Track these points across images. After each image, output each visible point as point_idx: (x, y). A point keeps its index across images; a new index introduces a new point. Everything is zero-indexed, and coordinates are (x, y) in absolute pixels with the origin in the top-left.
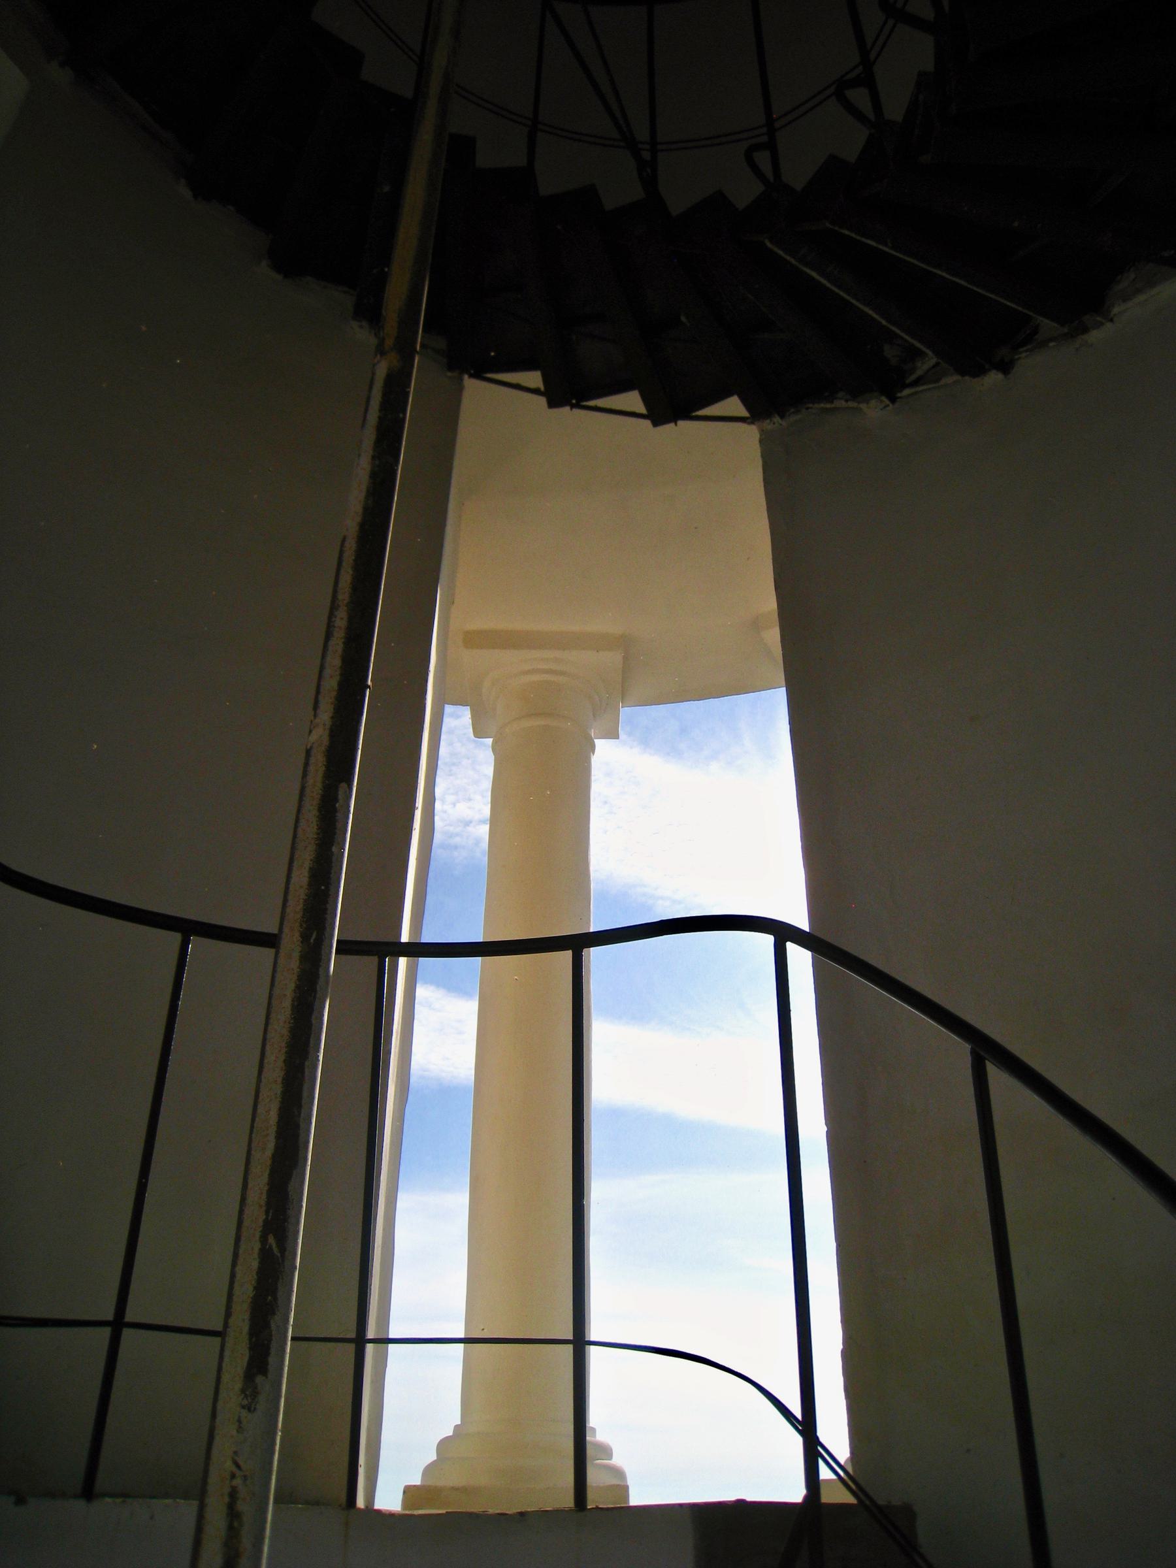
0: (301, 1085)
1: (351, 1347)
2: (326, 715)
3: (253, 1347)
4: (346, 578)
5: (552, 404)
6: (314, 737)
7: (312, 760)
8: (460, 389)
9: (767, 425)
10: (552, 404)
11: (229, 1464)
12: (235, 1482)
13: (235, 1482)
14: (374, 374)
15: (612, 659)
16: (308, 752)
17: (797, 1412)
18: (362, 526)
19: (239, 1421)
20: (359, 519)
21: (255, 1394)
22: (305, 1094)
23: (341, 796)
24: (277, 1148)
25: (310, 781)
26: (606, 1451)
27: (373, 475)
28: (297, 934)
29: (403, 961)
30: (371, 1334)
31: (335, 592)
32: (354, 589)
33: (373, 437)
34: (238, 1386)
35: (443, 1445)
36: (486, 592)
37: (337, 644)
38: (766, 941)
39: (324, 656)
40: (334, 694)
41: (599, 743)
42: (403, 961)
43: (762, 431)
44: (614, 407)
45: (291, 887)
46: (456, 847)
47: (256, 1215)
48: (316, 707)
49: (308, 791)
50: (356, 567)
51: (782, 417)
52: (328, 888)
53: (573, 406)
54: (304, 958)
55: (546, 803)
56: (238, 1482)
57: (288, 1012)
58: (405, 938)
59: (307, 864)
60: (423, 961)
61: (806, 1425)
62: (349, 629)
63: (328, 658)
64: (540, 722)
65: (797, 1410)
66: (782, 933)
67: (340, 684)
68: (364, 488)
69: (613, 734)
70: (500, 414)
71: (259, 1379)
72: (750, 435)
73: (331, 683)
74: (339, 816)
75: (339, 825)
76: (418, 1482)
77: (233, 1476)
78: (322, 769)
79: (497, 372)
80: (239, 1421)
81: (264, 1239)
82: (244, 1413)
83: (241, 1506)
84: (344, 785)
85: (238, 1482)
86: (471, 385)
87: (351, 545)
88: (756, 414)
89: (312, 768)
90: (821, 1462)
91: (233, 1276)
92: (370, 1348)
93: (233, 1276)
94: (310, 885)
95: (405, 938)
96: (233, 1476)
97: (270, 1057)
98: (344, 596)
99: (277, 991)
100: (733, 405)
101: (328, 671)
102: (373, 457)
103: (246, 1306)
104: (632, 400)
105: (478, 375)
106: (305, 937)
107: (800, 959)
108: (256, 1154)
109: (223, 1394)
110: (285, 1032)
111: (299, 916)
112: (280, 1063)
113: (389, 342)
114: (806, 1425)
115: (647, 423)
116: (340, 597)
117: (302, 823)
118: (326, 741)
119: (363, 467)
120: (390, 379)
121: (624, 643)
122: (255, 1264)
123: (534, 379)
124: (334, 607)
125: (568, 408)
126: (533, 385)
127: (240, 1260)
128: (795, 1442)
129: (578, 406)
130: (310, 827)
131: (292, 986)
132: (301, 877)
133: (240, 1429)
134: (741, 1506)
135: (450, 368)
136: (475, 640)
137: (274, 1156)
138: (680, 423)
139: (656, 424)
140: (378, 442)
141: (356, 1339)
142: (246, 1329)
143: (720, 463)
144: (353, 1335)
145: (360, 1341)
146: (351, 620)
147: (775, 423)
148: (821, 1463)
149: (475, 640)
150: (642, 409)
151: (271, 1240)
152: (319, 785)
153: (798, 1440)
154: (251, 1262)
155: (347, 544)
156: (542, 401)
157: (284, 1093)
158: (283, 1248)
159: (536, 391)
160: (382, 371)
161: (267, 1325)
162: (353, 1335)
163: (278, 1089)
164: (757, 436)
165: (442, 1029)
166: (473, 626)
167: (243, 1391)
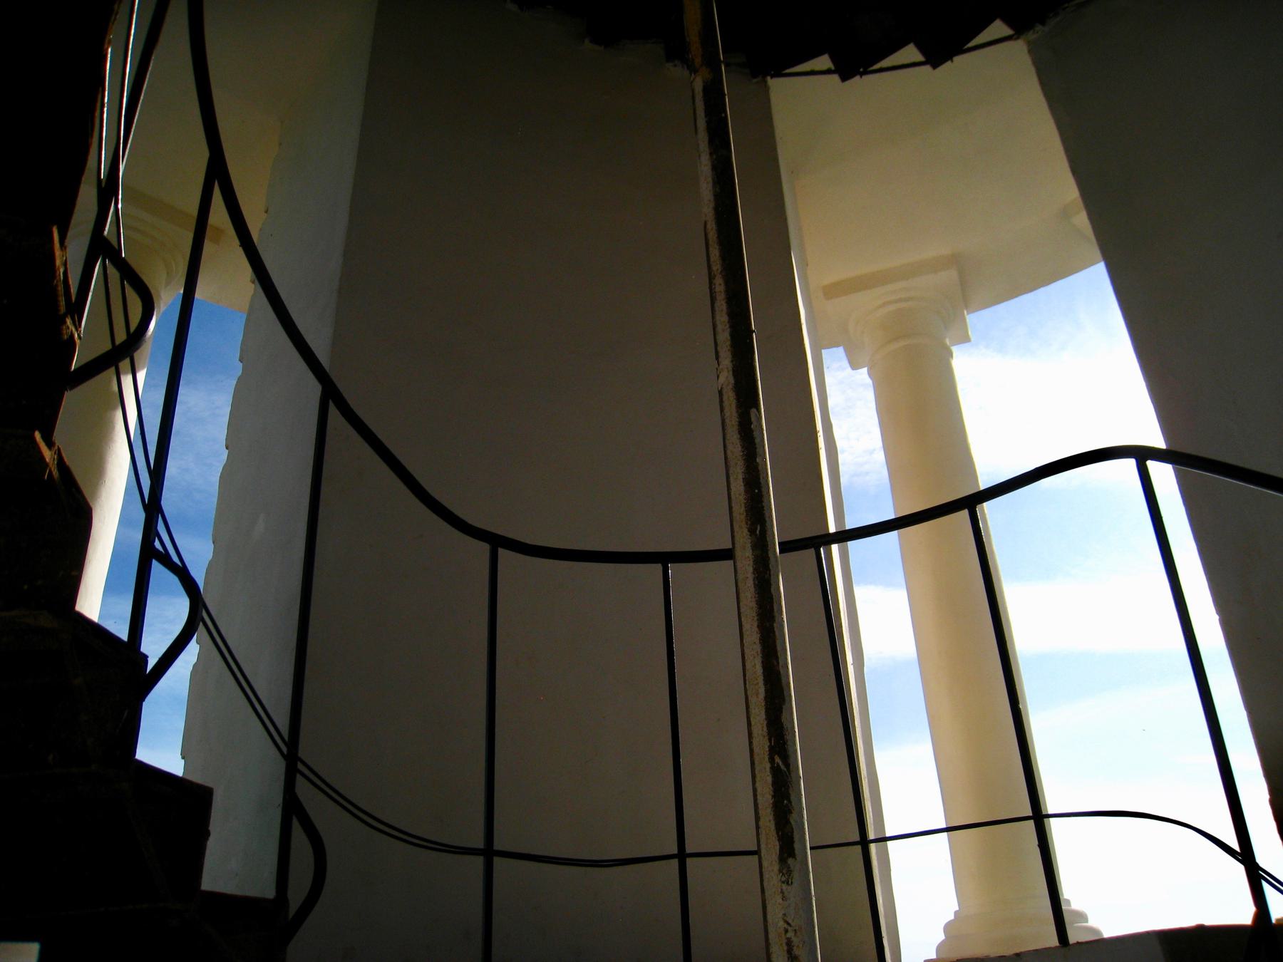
0: (774, 642)
1: (858, 848)
2: (726, 361)
3: (780, 839)
4: (715, 252)
5: (844, 78)
6: (722, 379)
7: (725, 398)
8: (766, 90)
9: (1031, 36)
10: (844, 78)
11: (781, 924)
12: (789, 935)
13: (789, 935)
14: (693, 91)
15: (949, 276)
16: (720, 393)
17: (1235, 845)
18: (716, 209)
19: (782, 892)
20: (712, 205)
21: (790, 872)
22: (779, 648)
23: (753, 419)
24: (766, 691)
25: (727, 414)
26: (1082, 916)
27: (714, 168)
28: (746, 531)
29: (835, 547)
30: (871, 836)
31: (709, 267)
32: (723, 258)
33: (706, 139)
34: (776, 867)
35: (948, 927)
36: (834, 250)
37: (721, 305)
38: (1130, 464)
39: (713, 317)
40: (728, 343)
41: (954, 349)
42: (835, 547)
43: (1029, 43)
44: (895, 64)
45: (733, 497)
46: (867, 473)
47: (762, 744)
48: (717, 358)
49: (727, 421)
50: (720, 243)
51: (1043, 23)
52: (760, 491)
53: (862, 74)
54: (754, 547)
55: (923, 412)
56: (790, 934)
57: (752, 589)
58: (832, 529)
59: (741, 477)
60: (850, 544)
61: (1245, 855)
62: (727, 291)
63: (718, 317)
64: (902, 343)
65: (1234, 844)
66: (1141, 455)
67: (732, 335)
68: (710, 179)
69: (965, 339)
70: (806, 104)
71: (790, 861)
72: (1018, 50)
73: (724, 336)
74: (756, 434)
75: (757, 441)
76: (934, 956)
77: (786, 931)
78: (734, 402)
79: (793, 66)
80: (782, 892)
81: (772, 760)
82: (784, 886)
83: (796, 951)
84: (754, 410)
85: (790, 934)
86: (775, 84)
87: (712, 226)
88: (1019, 28)
89: (726, 404)
90: (1264, 883)
91: (755, 790)
92: (873, 847)
93: (755, 790)
94: (746, 492)
95: (832, 529)
96: (786, 931)
97: (746, 626)
98: (717, 266)
99: (740, 577)
100: (998, 28)
101: (720, 328)
102: (711, 154)
103: (769, 810)
104: (910, 53)
105: (779, 74)
106: (752, 532)
107: (1163, 475)
108: (753, 700)
109: (766, 876)
110: (754, 604)
111: (743, 517)
112: (755, 629)
113: (698, 61)
114: (1245, 855)
115: (928, 68)
116: (714, 268)
117: (730, 447)
118: (732, 380)
119: (705, 166)
120: (706, 90)
121: (955, 261)
122: (769, 779)
123: (824, 62)
124: (711, 278)
125: (858, 77)
126: (825, 68)
127: (758, 779)
128: (1238, 870)
129: (866, 73)
130: (736, 449)
131: (751, 569)
132: (738, 487)
133: (784, 898)
134: (1201, 931)
135: (754, 77)
136: (833, 291)
137: (766, 698)
138: (956, 59)
139: (935, 66)
140: (711, 142)
141: (862, 842)
142: (773, 827)
143: (1000, 84)
144: (858, 839)
145: (864, 842)
146: (727, 283)
147: (1039, 31)
148: (1265, 884)
149: (833, 291)
150: (920, 58)
151: (777, 760)
152: (735, 414)
153: (1240, 869)
154: (765, 779)
155: (709, 226)
156: (836, 78)
157: (763, 651)
158: (787, 765)
159: (828, 72)
160: (698, 85)
161: (788, 822)
162: (858, 839)
163: (758, 648)
164: (1025, 49)
165: (882, 611)
166: (829, 279)
167: (780, 871)
